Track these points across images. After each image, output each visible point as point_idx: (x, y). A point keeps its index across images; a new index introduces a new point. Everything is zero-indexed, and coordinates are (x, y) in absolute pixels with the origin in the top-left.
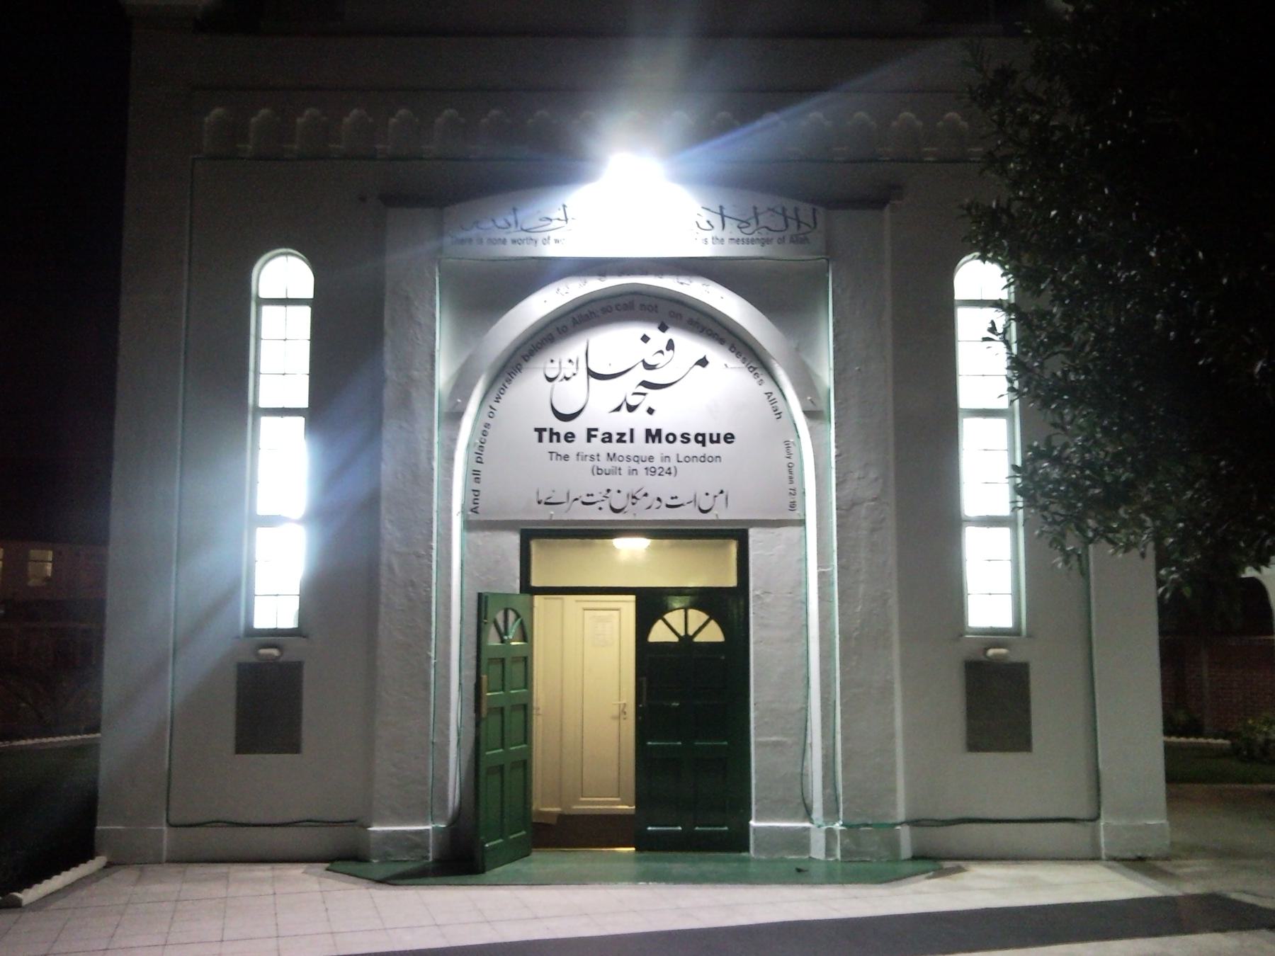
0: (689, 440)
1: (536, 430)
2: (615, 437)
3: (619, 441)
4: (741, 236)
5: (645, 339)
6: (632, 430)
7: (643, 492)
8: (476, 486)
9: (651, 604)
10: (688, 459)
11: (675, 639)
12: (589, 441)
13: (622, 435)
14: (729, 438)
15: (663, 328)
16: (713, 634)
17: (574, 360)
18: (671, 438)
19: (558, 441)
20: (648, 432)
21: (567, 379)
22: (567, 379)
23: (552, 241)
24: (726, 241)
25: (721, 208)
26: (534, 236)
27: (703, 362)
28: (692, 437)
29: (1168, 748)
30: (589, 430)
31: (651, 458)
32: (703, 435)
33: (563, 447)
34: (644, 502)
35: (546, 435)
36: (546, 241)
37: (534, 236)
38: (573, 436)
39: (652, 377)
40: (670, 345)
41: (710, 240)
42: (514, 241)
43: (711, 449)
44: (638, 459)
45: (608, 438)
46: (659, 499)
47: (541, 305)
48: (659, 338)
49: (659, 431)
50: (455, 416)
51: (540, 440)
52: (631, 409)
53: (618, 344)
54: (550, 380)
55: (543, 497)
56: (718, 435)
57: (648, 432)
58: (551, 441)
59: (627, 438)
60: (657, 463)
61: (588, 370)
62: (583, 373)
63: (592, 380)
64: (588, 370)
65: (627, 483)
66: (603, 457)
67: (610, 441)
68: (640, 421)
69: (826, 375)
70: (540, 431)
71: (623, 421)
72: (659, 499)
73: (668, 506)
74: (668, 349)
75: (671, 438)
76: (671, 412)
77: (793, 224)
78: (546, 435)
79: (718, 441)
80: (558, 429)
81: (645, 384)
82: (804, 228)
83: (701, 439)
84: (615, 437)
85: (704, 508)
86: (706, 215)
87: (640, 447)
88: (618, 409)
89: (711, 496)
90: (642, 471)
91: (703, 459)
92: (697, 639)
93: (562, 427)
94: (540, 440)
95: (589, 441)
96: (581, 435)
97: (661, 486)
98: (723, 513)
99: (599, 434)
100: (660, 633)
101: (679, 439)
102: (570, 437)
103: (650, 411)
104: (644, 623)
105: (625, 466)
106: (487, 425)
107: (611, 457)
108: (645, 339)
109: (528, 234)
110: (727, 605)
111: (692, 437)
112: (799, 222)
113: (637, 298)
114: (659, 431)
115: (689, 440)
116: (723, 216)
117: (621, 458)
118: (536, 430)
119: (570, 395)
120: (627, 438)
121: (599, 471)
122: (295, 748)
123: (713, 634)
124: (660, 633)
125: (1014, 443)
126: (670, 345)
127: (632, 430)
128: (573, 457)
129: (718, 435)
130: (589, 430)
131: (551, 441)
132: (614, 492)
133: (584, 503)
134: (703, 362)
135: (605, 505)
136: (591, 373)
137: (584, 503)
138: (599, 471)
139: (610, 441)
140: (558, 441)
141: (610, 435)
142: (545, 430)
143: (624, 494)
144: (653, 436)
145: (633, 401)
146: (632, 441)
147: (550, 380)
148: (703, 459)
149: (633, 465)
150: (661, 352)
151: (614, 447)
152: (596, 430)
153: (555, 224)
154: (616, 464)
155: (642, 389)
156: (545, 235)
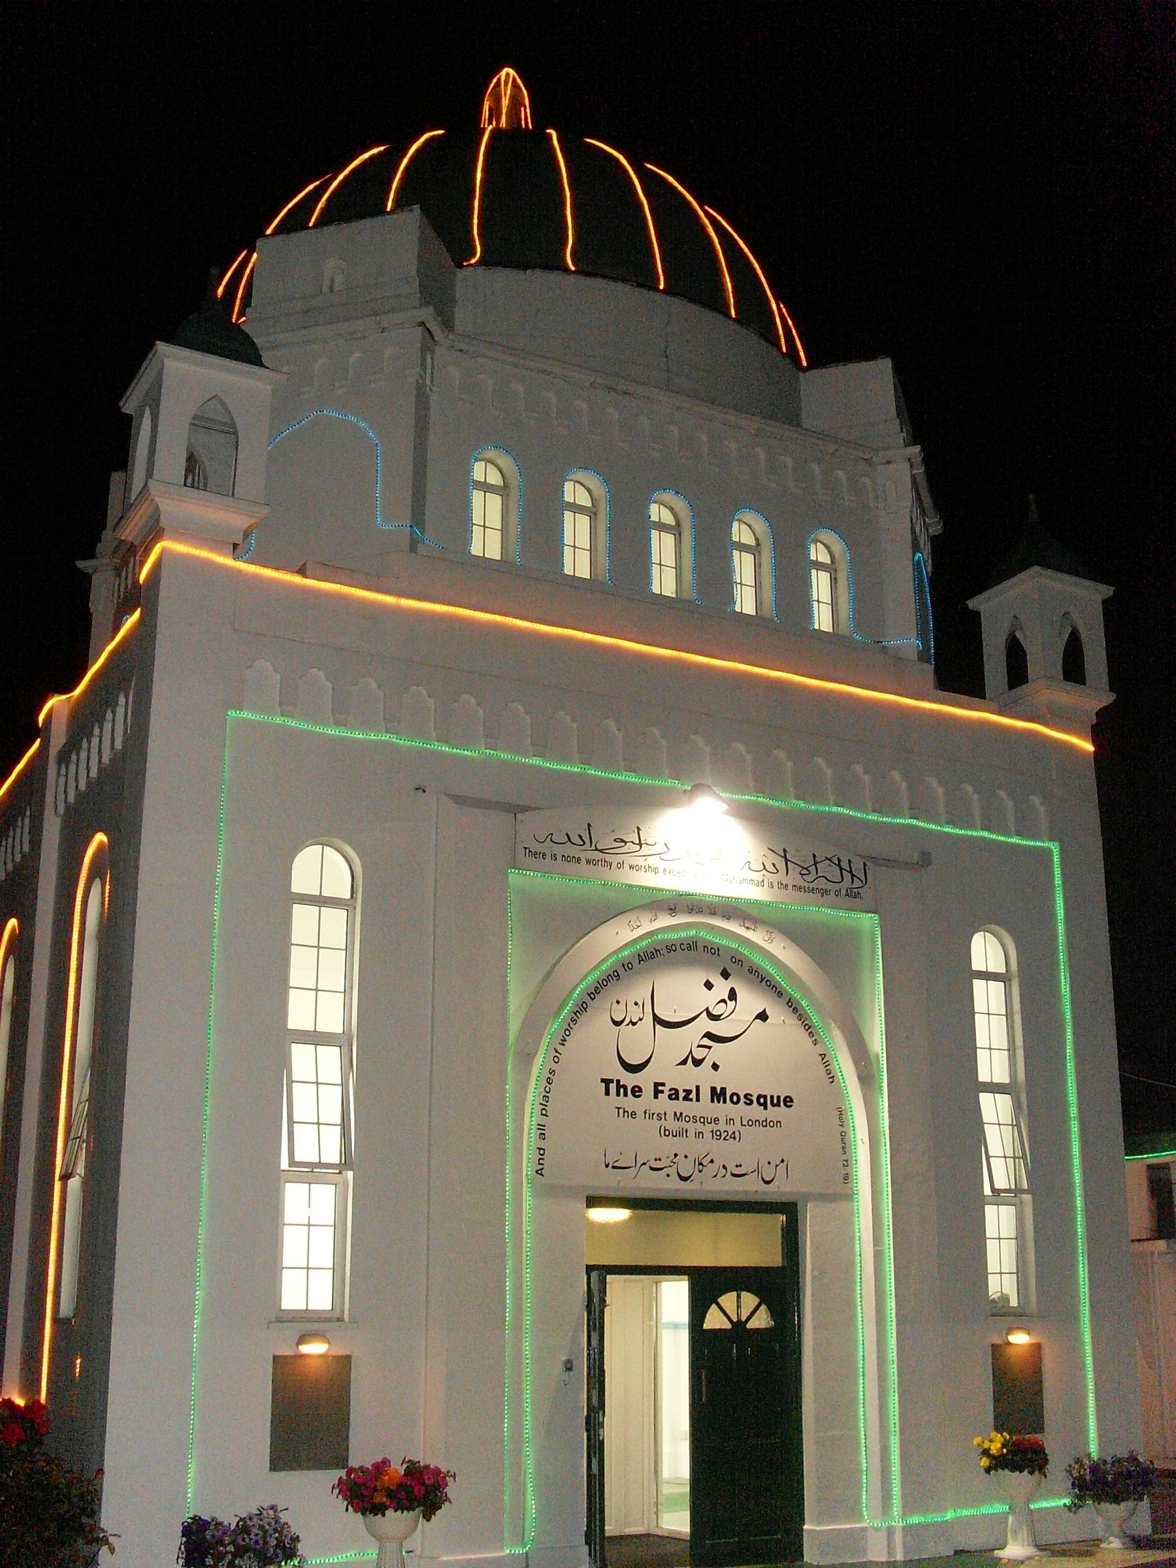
0: (751, 1102)
1: (603, 1080)
2: (682, 1095)
3: (686, 1098)
4: (800, 882)
5: (709, 985)
6: (698, 1088)
7: (708, 1159)
8: (542, 1144)
9: (707, 1286)
10: (752, 1123)
11: (728, 1326)
12: (656, 1097)
13: (688, 1092)
14: (788, 1101)
15: (725, 975)
16: (762, 1320)
17: (641, 1004)
18: (735, 1099)
19: (626, 1095)
20: (713, 1089)
21: (634, 1024)
22: (634, 1024)
23: (626, 866)
24: (790, 887)
25: (785, 851)
26: (608, 858)
27: (763, 1016)
28: (754, 1099)
29: (1041, 1430)
30: (656, 1085)
31: (716, 1120)
32: (765, 1097)
33: (629, 1102)
34: (710, 1170)
35: (613, 1087)
36: (620, 865)
37: (608, 858)
38: (640, 1090)
39: (717, 1028)
40: (733, 995)
41: (775, 885)
42: (588, 862)
43: (772, 1113)
44: (704, 1121)
45: (674, 1095)
46: (724, 1167)
47: (620, 936)
48: (722, 988)
49: (723, 1090)
50: (526, 1057)
51: (607, 1093)
52: (697, 1063)
53: (684, 991)
54: (617, 1024)
55: (611, 1161)
56: (779, 1097)
57: (713, 1089)
58: (618, 1094)
59: (693, 1096)
60: (722, 1126)
61: (654, 1015)
62: (649, 1019)
63: (658, 1026)
64: (654, 1015)
65: (693, 1147)
66: (670, 1116)
67: (677, 1098)
68: (704, 1078)
69: (877, 1042)
70: (607, 1082)
71: (687, 1078)
72: (724, 1167)
73: (733, 1175)
74: (731, 999)
75: (735, 1099)
76: (738, 1068)
77: (847, 875)
78: (613, 1087)
79: (778, 1105)
80: (624, 1081)
81: (709, 1035)
82: (857, 883)
83: (763, 1101)
84: (682, 1095)
85: (767, 1179)
86: (774, 858)
87: (706, 1108)
88: (684, 1062)
89: (773, 1165)
90: (708, 1135)
91: (765, 1123)
92: (749, 1326)
93: (629, 1080)
94: (607, 1093)
95: (656, 1097)
96: (648, 1090)
97: (726, 1153)
98: (781, 1189)
99: (666, 1089)
100: (714, 1320)
101: (743, 1099)
102: (637, 1091)
103: (715, 1067)
104: (698, 1309)
105: (692, 1127)
106: (552, 1072)
107: (678, 1117)
108: (709, 985)
109: (602, 856)
110: (778, 1286)
111: (754, 1099)
112: (853, 876)
113: (698, 940)
114: (723, 1090)
115: (751, 1102)
116: (787, 860)
117: (688, 1119)
118: (603, 1080)
119: (638, 1041)
120: (693, 1096)
121: (667, 1133)
122: (275, 1466)
123: (762, 1320)
124: (714, 1320)
125: (347, 1198)
126: (733, 995)
127: (698, 1088)
128: (640, 1114)
129: (779, 1097)
130: (656, 1085)
131: (618, 1094)
132: (681, 1156)
133: (652, 1169)
134: (763, 1016)
135: (672, 1171)
136: (657, 1020)
137: (652, 1169)
138: (667, 1133)
139: (677, 1098)
140: (626, 1095)
141: (677, 1091)
142: (612, 1081)
143: (691, 1159)
144: (718, 1095)
145: (699, 1054)
146: (698, 1100)
147: (617, 1024)
148: (765, 1123)
149: (699, 1127)
150: (723, 1001)
151: (680, 1105)
152: (663, 1084)
153: (630, 847)
154: (683, 1124)
155: (706, 1041)
156: (620, 858)
